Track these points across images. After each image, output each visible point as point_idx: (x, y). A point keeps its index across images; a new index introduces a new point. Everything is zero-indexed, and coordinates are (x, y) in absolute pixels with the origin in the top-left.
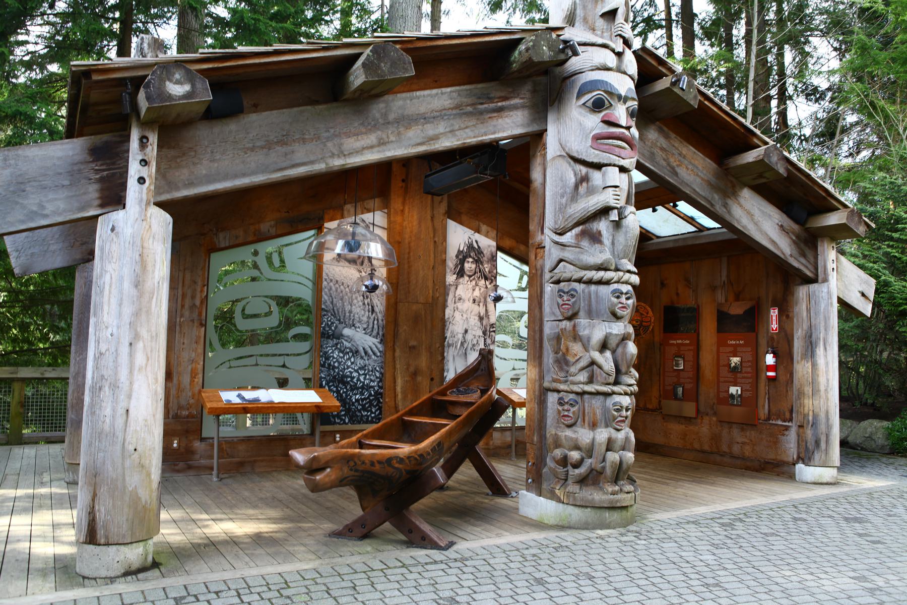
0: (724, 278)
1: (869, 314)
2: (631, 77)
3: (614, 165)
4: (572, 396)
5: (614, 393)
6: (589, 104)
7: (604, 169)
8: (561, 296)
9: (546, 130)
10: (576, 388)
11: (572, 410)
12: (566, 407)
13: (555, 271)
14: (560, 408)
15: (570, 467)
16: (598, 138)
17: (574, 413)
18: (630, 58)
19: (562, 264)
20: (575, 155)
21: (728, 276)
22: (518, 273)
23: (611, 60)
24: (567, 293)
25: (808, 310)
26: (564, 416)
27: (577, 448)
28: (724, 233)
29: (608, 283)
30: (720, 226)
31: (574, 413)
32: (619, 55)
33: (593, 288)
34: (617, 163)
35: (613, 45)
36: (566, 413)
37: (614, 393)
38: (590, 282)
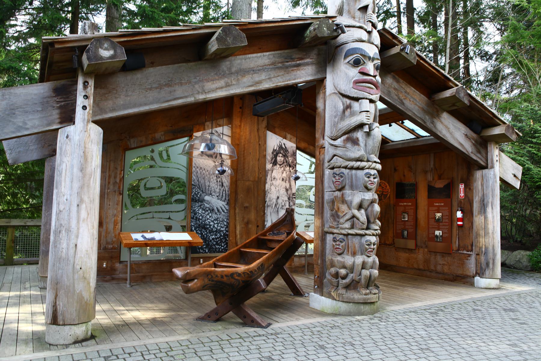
0: (432, 166)
2: (376, 46)
6: (352, 62)
7: (360, 101)
8: (334, 177)
9: (326, 78)
10: (344, 232)
11: (341, 244)
12: (338, 243)
14: (334, 244)
15: (340, 279)
16: (357, 82)
17: (342, 246)
19: (335, 157)
20: (343, 92)
21: (434, 165)
23: (364, 36)
26: (337, 248)
31: (342, 246)
32: (369, 33)
33: (354, 172)
34: (368, 97)
35: (365, 27)
36: (338, 247)
37: (366, 234)
38: (352, 168)
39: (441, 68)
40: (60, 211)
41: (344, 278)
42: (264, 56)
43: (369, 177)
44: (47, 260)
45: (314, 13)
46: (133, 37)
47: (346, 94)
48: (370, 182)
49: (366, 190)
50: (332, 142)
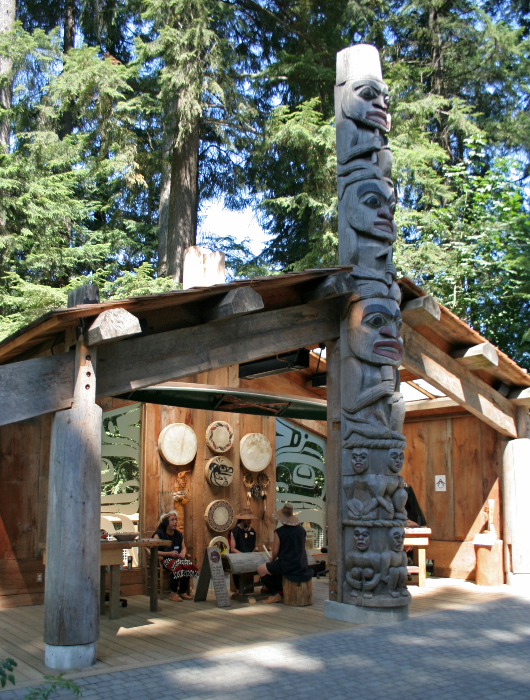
0: (449, 435)
1: (439, 319)
2: (398, 301)
3: (389, 365)
4: (364, 530)
5: (394, 526)
6: (371, 321)
7: (383, 367)
8: (354, 458)
9: (339, 338)
10: (369, 523)
11: (366, 539)
12: (361, 537)
13: (350, 439)
14: (356, 538)
15: (364, 581)
16: (378, 345)
17: (366, 541)
18: (396, 287)
19: (353, 436)
20: (362, 357)
21: (452, 433)
22: (291, 432)
23: (385, 291)
24: (360, 455)
25: (457, 418)
26: (359, 544)
27: (371, 566)
28: (448, 401)
29: (385, 448)
30: (445, 395)
31: (366, 541)
32: (389, 286)
33: (377, 452)
34: (392, 363)
35: (386, 280)
36: (361, 542)
37: (394, 526)
38: (376, 448)
39: (44, 282)
40: (45, 390)
41: (369, 579)
42: (272, 315)
43: (395, 458)
44: (38, 416)
45: (104, 282)
46: (388, 342)
47: (374, 361)
48: (396, 464)
49: (389, 472)
50: (349, 416)
